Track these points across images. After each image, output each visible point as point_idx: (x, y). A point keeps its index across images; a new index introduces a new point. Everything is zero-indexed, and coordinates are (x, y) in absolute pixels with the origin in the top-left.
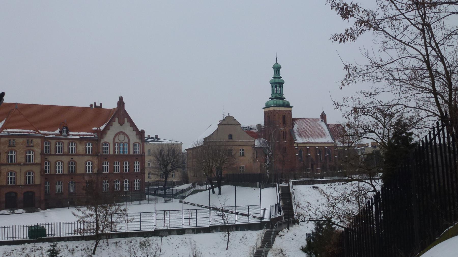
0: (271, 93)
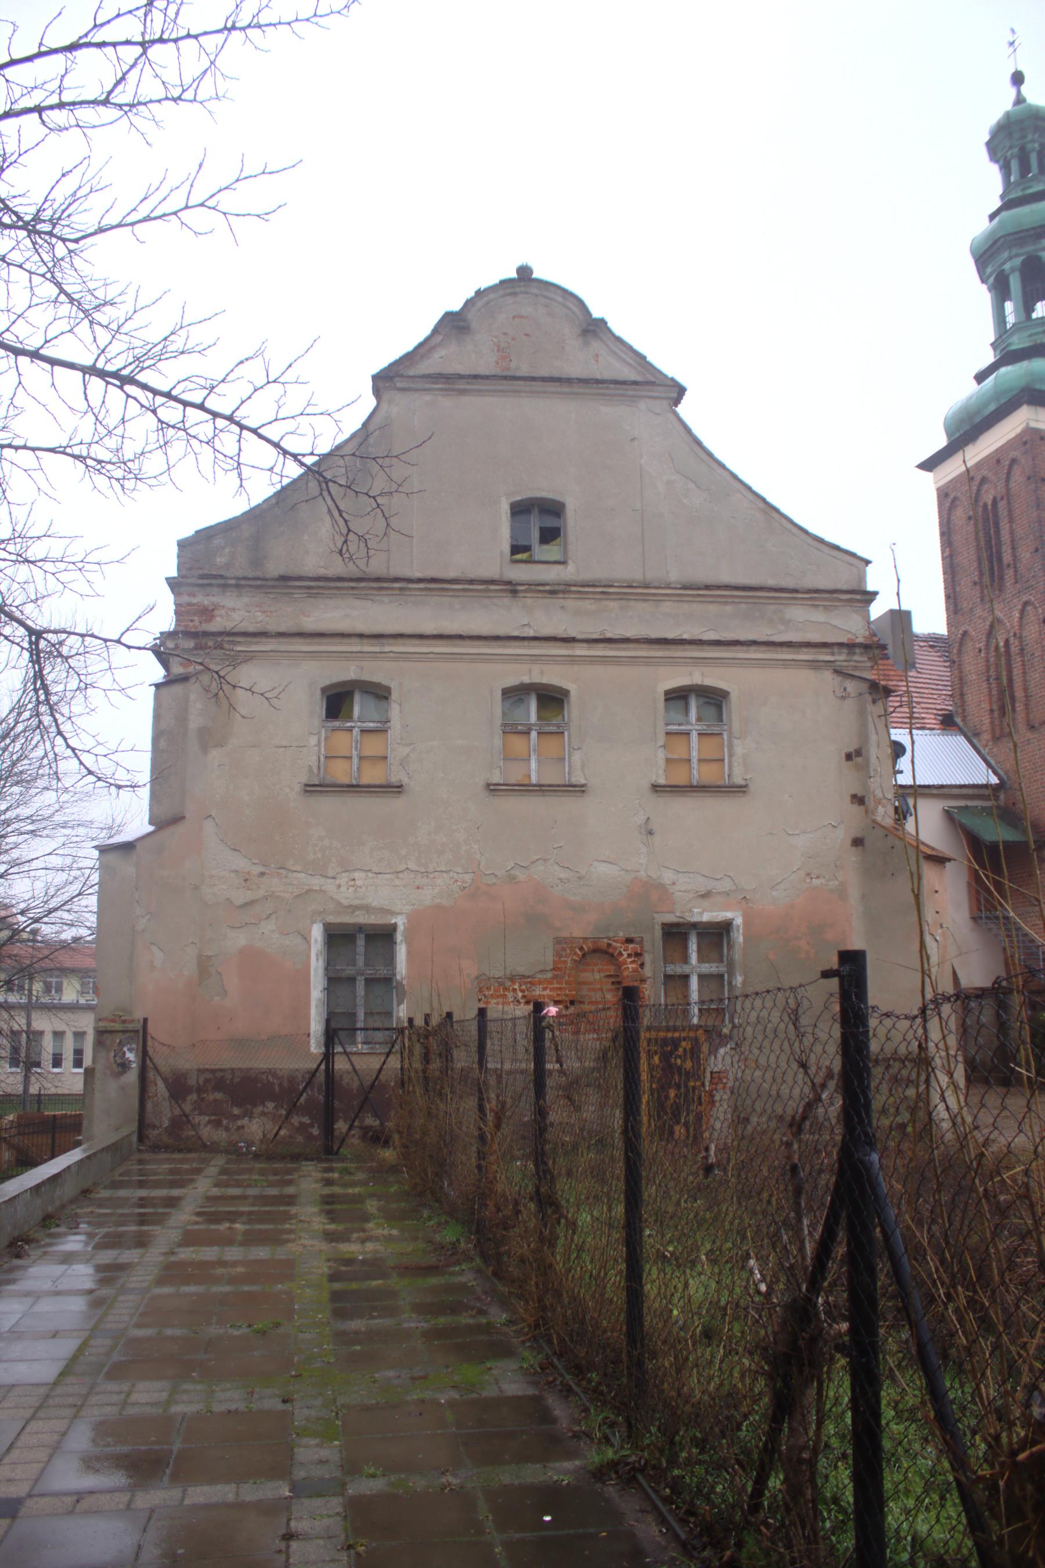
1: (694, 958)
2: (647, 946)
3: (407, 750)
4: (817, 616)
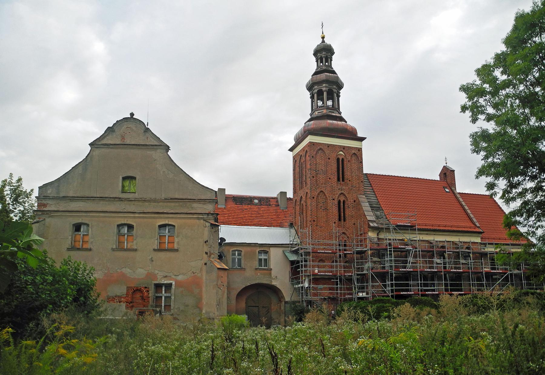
1: (163, 292)
2: (150, 289)
3: (92, 240)
4: (200, 205)
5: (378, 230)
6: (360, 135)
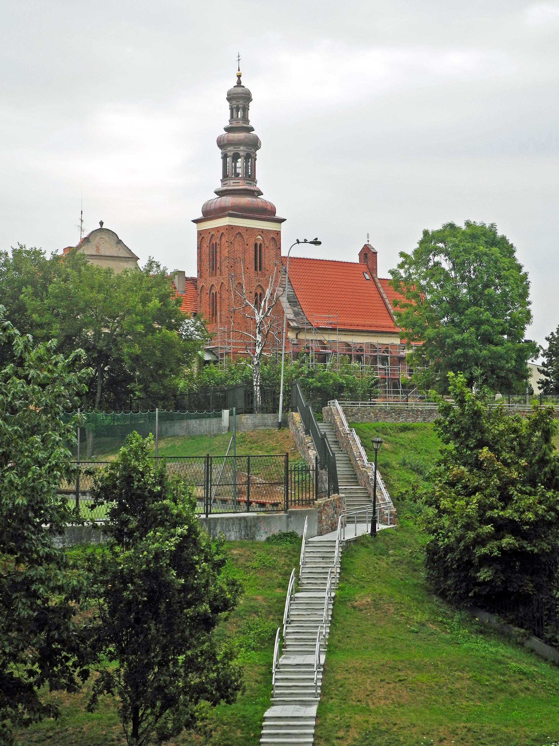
0: (229, 118)
5: (298, 330)
6: (279, 215)
